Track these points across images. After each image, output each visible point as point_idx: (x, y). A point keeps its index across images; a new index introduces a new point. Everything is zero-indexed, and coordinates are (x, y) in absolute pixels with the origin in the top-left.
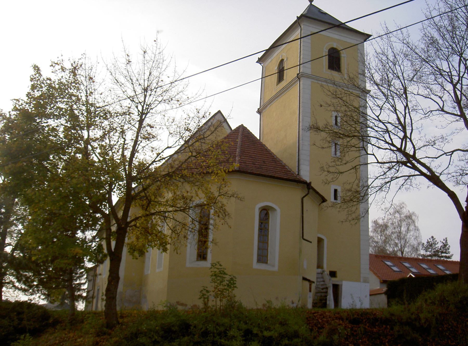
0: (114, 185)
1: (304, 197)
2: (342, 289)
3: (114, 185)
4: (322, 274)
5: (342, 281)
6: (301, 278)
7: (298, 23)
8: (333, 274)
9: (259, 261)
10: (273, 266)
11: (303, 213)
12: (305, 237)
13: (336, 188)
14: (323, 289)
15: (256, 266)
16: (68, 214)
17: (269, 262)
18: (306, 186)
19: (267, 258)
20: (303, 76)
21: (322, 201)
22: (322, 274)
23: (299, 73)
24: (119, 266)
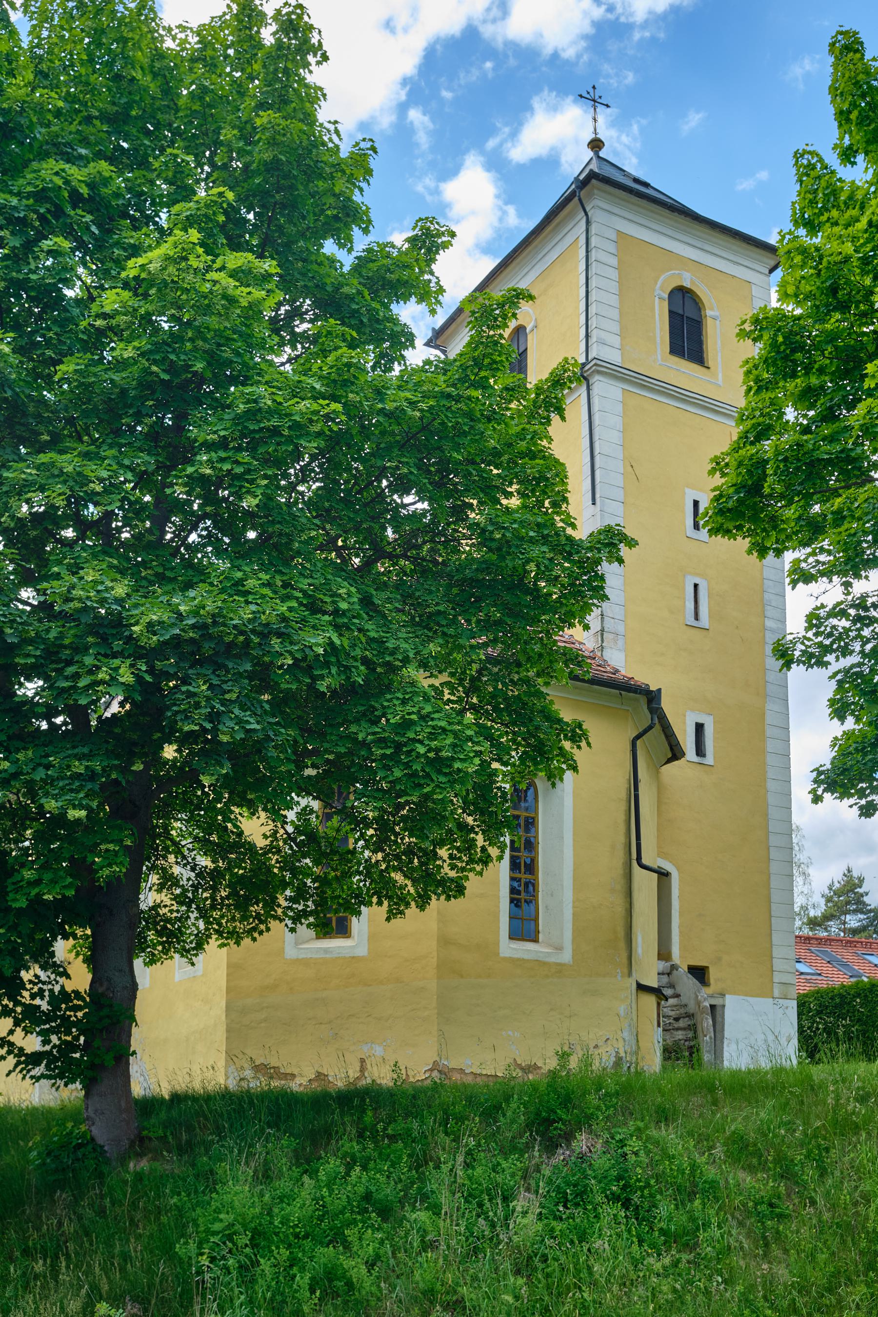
0: (86, 750)
1: (638, 737)
2: (723, 1018)
3: (86, 750)
4: (669, 974)
5: (723, 995)
6: (634, 986)
7: (580, 200)
8: (699, 973)
9: (516, 935)
10: (559, 948)
11: (636, 788)
12: (645, 861)
13: (700, 721)
14: (677, 1019)
15: (510, 949)
16: (153, 204)
17: (541, 936)
18: (643, 700)
19: (537, 925)
20: (599, 372)
21: (670, 755)
22: (669, 974)
23: (584, 361)
24: (574, 855)
